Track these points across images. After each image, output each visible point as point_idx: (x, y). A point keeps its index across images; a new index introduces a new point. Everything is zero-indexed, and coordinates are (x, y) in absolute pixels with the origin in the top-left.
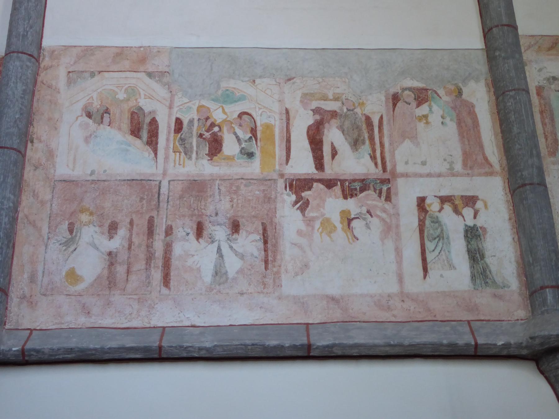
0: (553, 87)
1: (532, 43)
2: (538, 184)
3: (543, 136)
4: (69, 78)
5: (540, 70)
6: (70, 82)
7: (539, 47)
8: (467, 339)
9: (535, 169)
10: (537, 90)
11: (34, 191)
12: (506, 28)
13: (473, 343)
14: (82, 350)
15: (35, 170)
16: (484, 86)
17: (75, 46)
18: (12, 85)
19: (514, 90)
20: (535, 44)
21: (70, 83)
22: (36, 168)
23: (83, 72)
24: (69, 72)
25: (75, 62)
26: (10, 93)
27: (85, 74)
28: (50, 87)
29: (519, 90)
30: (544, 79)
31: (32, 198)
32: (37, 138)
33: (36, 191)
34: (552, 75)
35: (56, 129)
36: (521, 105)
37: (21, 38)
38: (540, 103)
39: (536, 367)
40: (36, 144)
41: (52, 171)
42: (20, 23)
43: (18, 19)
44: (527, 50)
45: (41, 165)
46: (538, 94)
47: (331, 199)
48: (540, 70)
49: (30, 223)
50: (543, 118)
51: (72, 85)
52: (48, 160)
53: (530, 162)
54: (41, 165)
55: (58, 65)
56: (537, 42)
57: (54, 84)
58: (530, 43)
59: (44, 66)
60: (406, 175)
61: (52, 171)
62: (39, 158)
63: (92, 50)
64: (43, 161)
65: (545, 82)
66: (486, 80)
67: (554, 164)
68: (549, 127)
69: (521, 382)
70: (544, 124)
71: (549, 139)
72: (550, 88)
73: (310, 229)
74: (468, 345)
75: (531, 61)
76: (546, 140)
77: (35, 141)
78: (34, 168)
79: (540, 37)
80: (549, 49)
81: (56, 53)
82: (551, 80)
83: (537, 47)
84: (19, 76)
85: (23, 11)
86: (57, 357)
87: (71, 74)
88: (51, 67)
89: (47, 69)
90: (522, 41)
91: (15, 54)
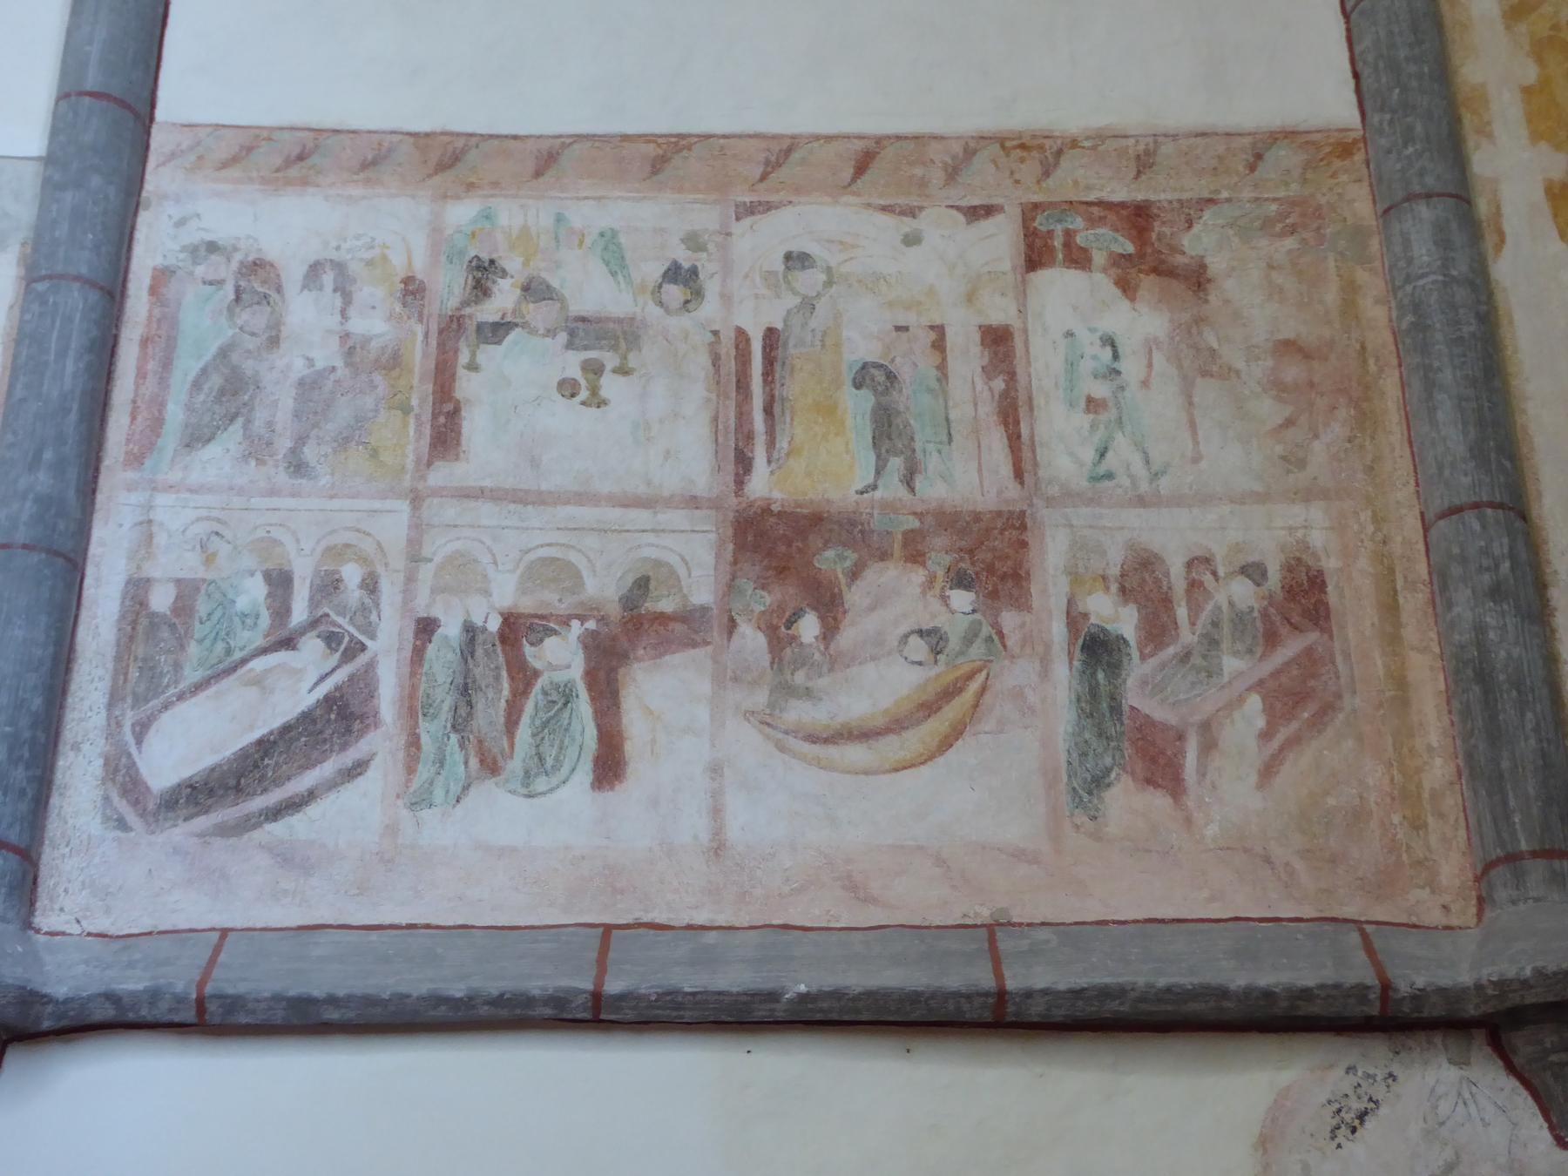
0: (200, 270)
1: (184, 147)
2: (25, 547)
3: (129, 408)
5: (181, 223)
7: (200, 158)
8: (1359, 972)
9: (28, 504)
10: (154, 278)
12: (87, 100)
13: (1371, 979)
16: (15, 261)
19: (50, 277)
20: (191, 149)
29: (61, 277)
30: (184, 249)
34: (209, 237)
36: (53, 322)
38: (150, 316)
39: (1500, 1063)
44: (164, 164)
46: (154, 290)
48: (181, 223)
50: (143, 358)
53: (23, 483)
56: (198, 143)
58: (179, 145)
60: (693, 502)
65: (182, 256)
66: (23, 244)
67: (129, 490)
68: (150, 386)
69: (1463, 1105)
70: (141, 375)
71: (140, 418)
72: (191, 273)
73: (1326, 636)
74: (1361, 991)
75: (165, 197)
76: (133, 418)
79: (209, 130)
80: (224, 165)
82: (203, 252)
83: (193, 158)
90: (158, 139)
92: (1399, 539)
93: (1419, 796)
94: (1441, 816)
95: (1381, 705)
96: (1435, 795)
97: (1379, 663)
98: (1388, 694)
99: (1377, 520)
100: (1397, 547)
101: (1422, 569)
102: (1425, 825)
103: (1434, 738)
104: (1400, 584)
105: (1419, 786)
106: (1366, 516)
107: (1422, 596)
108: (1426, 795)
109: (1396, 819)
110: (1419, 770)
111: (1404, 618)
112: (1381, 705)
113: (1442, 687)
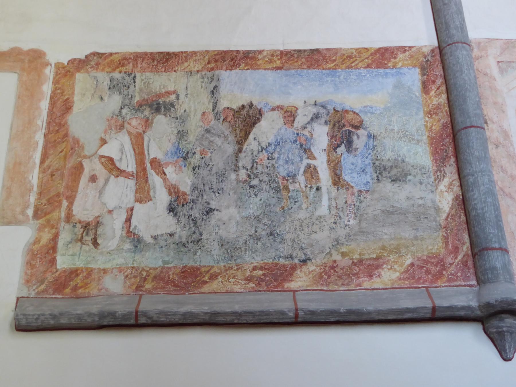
4: (500, 67)
6: (502, 71)
11: (502, 167)
14: (262, 313)
15: (496, 148)
17: (497, 39)
18: (466, 71)
21: (503, 72)
22: (497, 146)
23: (511, 62)
24: (498, 62)
25: (501, 54)
26: (466, 78)
27: (512, 64)
28: (486, 74)
31: (501, 173)
32: (490, 120)
33: (504, 167)
35: (503, 112)
37: (460, 30)
40: (491, 125)
41: (512, 150)
42: (455, 16)
43: (452, 13)
45: (501, 144)
47: (406, 186)
49: (506, 195)
51: (504, 73)
52: (505, 139)
54: (501, 144)
55: (487, 56)
57: (489, 72)
59: (475, 56)
61: (512, 150)
62: (497, 137)
63: (512, 43)
64: (502, 140)
69: (468, 342)
77: (488, 122)
78: (495, 146)
81: (482, 44)
84: (469, 64)
85: (454, 6)
86: (319, 317)
87: (500, 64)
88: (481, 57)
89: (478, 59)
91: (460, 44)
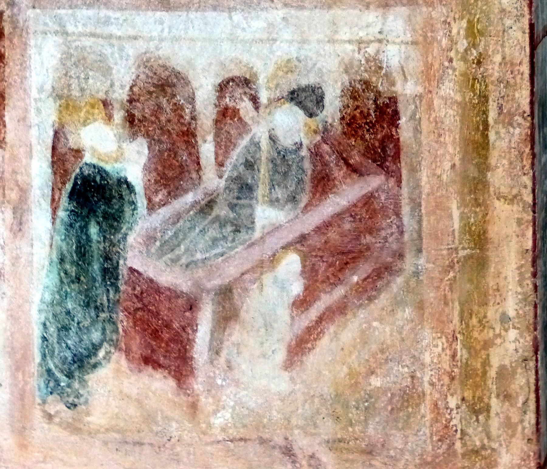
92: (498, 58)
93: (485, 373)
94: (507, 397)
95: (451, 266)
96: (504, 374)
97: (456, 214)
98: (462, 253)
99: (472, 33)
100: (494, 69)
101: (523, 96)
102: (487, 408)
103: (511, 307)
104: (492, 115)
105: (486, 363)
106: (459, 28)
107: (520, 130)
108: (492, 373)
109: (453, 402)
110: (487, 345)
111: (494, 159)
112: (451, 266)
113: (529, 244)
